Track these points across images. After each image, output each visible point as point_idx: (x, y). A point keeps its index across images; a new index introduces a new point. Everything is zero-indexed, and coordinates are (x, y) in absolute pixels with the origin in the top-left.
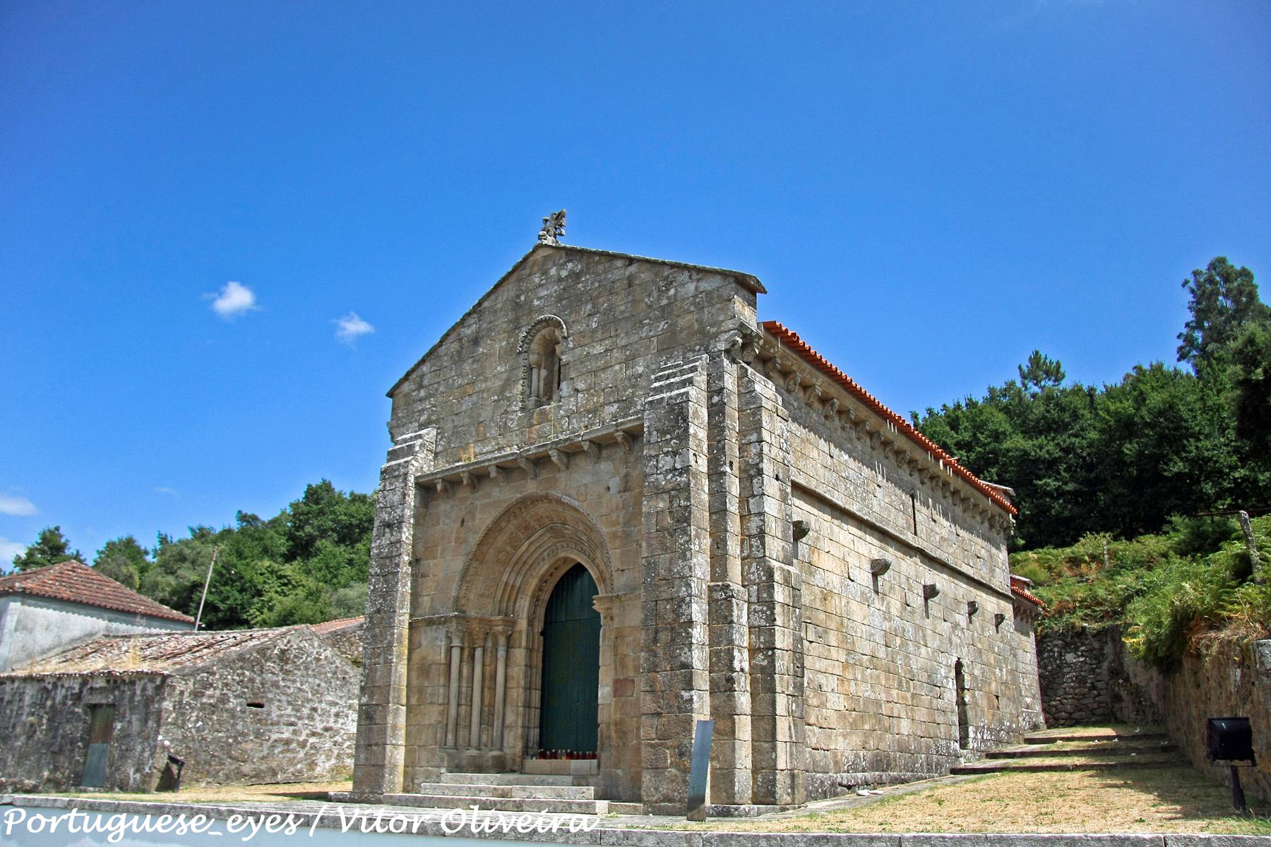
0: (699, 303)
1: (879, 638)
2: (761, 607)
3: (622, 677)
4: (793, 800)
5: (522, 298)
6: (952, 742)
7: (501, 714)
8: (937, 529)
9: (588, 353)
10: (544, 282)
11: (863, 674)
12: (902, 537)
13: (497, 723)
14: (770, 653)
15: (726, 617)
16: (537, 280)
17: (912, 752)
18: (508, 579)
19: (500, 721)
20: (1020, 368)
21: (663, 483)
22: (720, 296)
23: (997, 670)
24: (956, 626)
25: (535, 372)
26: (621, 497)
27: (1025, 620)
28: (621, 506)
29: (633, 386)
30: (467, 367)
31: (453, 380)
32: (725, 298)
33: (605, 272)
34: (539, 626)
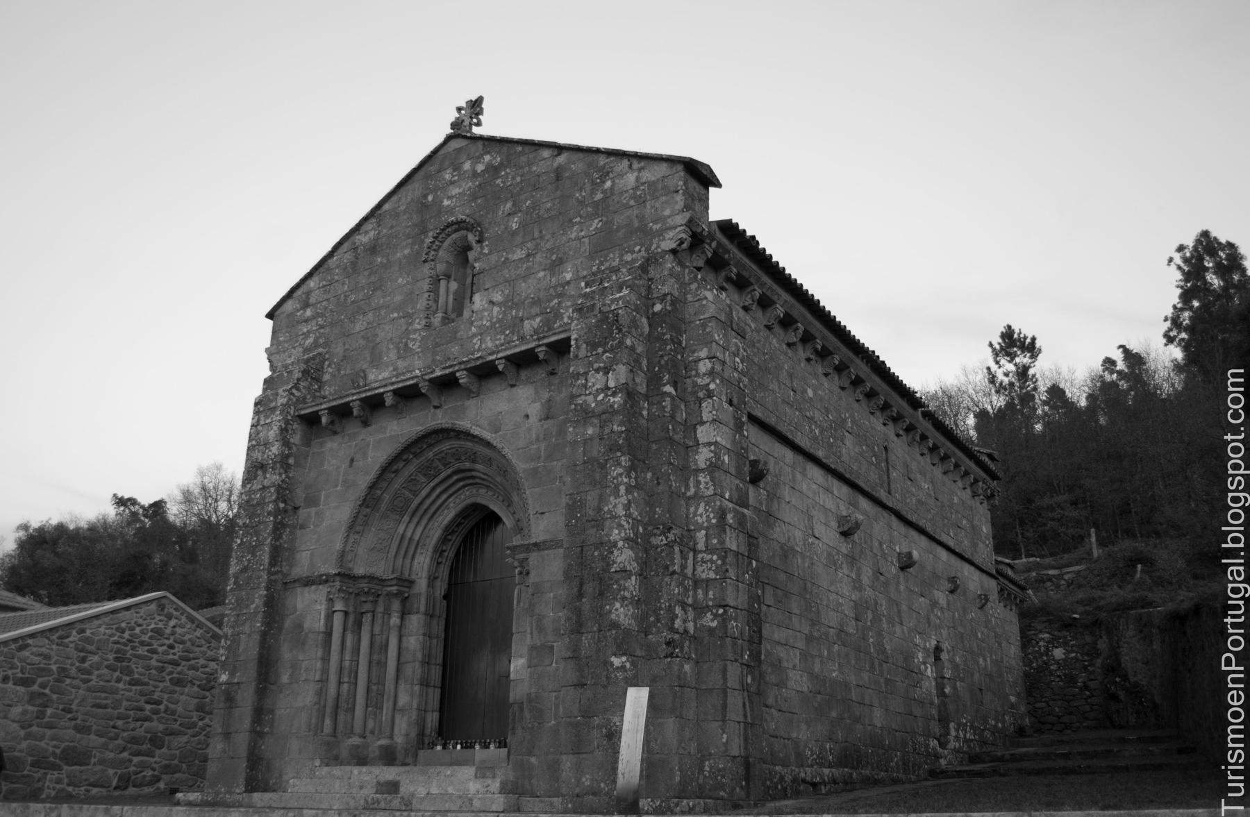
0: (640, 196)
1: (848, 610)
2: (710, 556)
3: (539, 643)
4: (748, 795)
5: (430, 198)
6: (931, 740)
7: (392, 693)
8: (914, 490)
9: (507, 259)
10: (456, 178)
11: (829, 650)
12: (874, 493)
13: (388, 706)
14: (721, 611)
15: (667, 567)
16: (448, 177)
17: (887, 748)
18: (405, 531)
19: (391, 703)
20: (991, 345)
21: (593, 405)
22: (665, 187)
23: (981, 660)
24: (934, 604)
25: (443, 283)
26: (542, 426)
27: (1009, 607)
28: (542, 436)
29: (560, 296)
30: (363, 280)
31: (345, 296)
32: (672, 189)
33: (529, 164)
34: (441, 588)
